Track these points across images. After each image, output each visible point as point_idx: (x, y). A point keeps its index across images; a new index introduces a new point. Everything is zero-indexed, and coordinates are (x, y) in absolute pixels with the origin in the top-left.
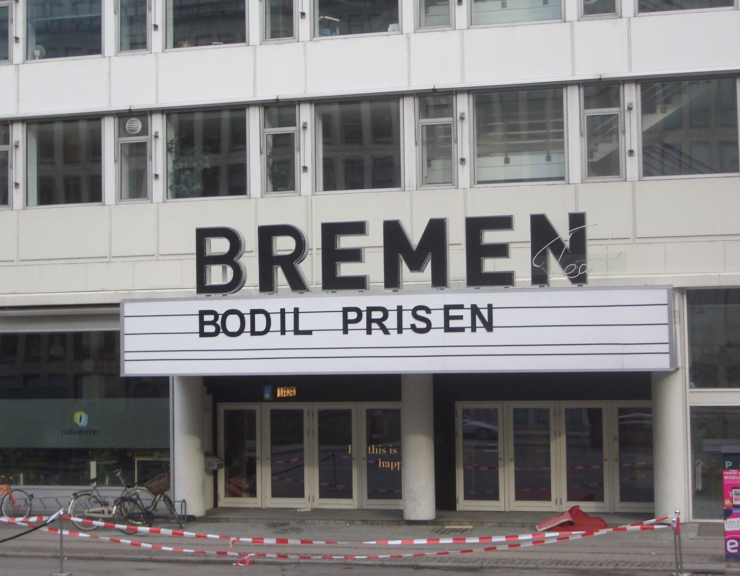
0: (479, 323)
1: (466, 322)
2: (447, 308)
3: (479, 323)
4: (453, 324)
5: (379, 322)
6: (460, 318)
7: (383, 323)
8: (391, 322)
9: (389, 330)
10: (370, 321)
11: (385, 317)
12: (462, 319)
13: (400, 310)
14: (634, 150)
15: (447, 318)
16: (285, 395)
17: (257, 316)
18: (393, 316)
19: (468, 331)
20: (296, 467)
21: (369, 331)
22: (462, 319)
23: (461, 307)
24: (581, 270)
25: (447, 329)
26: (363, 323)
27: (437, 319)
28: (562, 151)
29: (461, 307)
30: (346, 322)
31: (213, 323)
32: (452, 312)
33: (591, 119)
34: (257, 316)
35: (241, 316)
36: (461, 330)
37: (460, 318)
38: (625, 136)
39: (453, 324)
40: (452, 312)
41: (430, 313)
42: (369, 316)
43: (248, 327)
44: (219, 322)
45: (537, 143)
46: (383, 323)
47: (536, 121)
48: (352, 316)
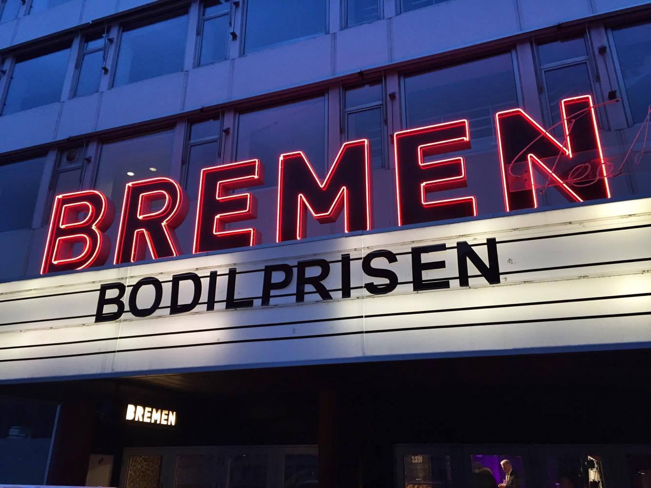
0: (472, 269)
1: (452, 270)
2: (417, 253)
3: (472, 269)
4: (428, 275)
5: (316, 282)
6: (441, 265)
7: (323, 282)
8: (334, 281)
9: (330, 293)
10: (303, 281)
11: (325, 273)
12: (444, 267)
13: (346, 260)
14: (411, 247)
15: (418, 267)
16: (148, 420)
17: (182, 283)
18: (336, 270)
19: (454, 284)
20: (608, 75)
21: (300, 296)
22: (444, 267)
23: (442, 247)
24: (319, 178)
25: (419, 285)
26: (292, 288)
27: (403, 268)
28: (566, 104)
29: (442, 247)
30: (268, 286)
31: (117, 301)
32: (425, 258)
33: (540, 134)
34: (182, 283)
35: (157, 284)
36: (443, 284)
37: (441, 265)
38: (600, 85)
39: (428, 275)
40: (425, 258)
41: (396, 260)
42: (301, 273)
43: (166, 300)
44: (125, 299)
45: (530, 147)
46: (323, 282)
47: (528, 146)
48: (278, 277)
